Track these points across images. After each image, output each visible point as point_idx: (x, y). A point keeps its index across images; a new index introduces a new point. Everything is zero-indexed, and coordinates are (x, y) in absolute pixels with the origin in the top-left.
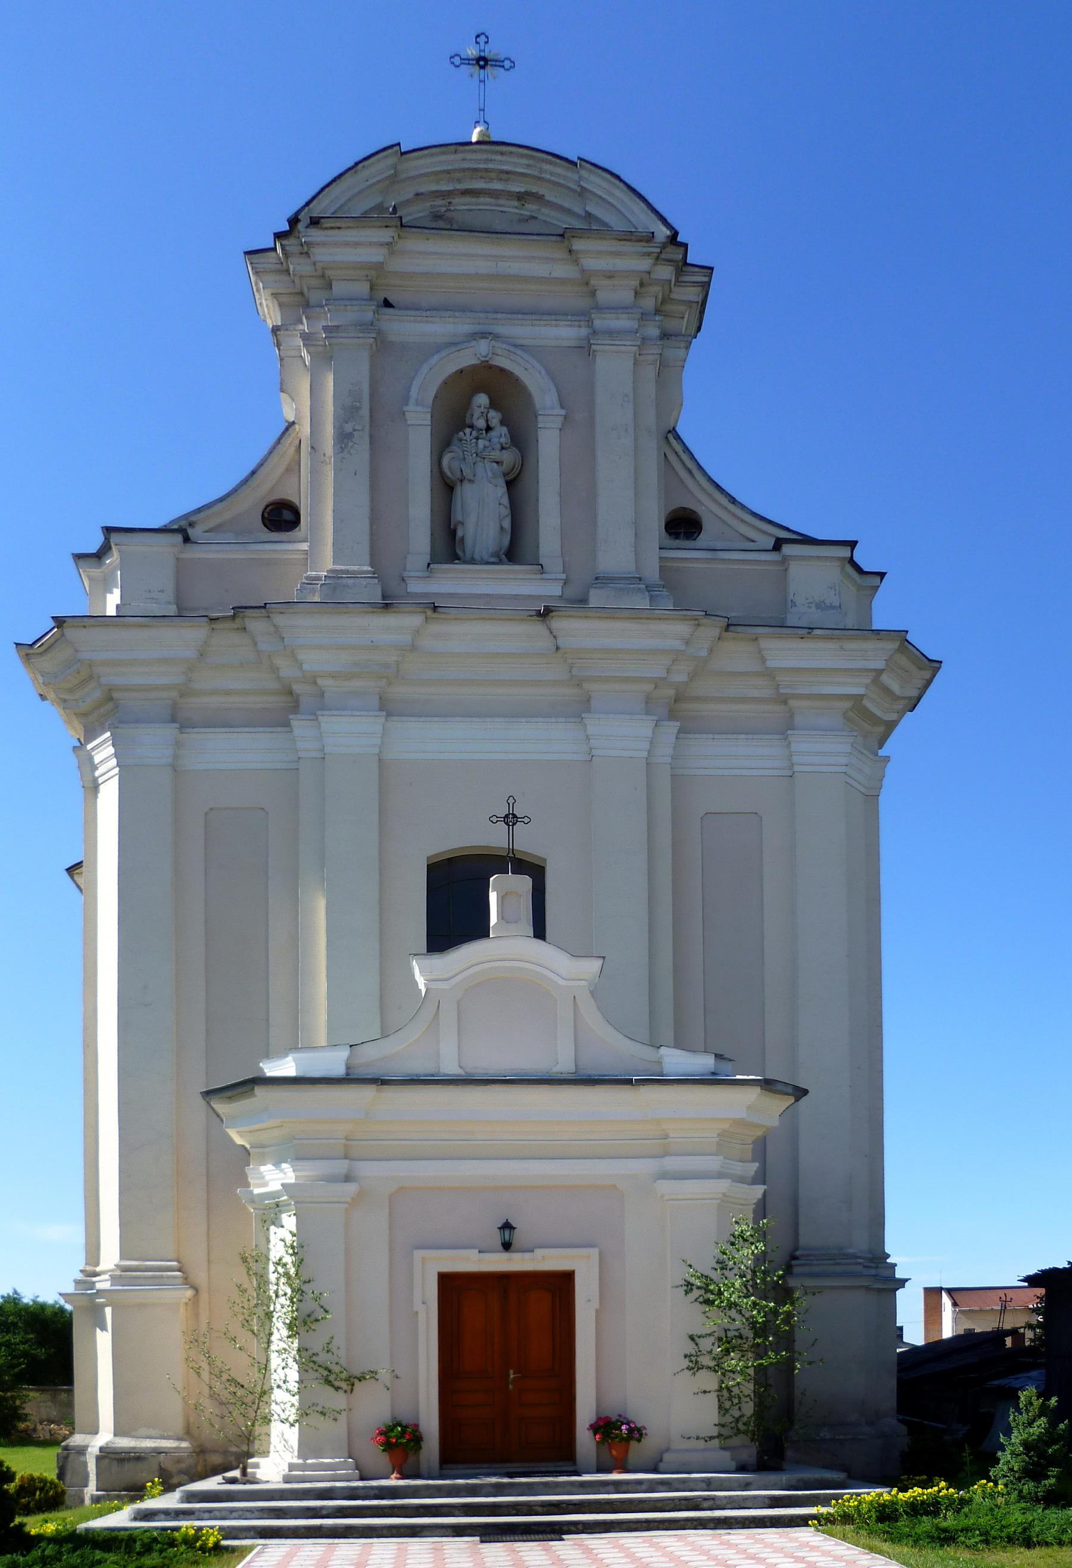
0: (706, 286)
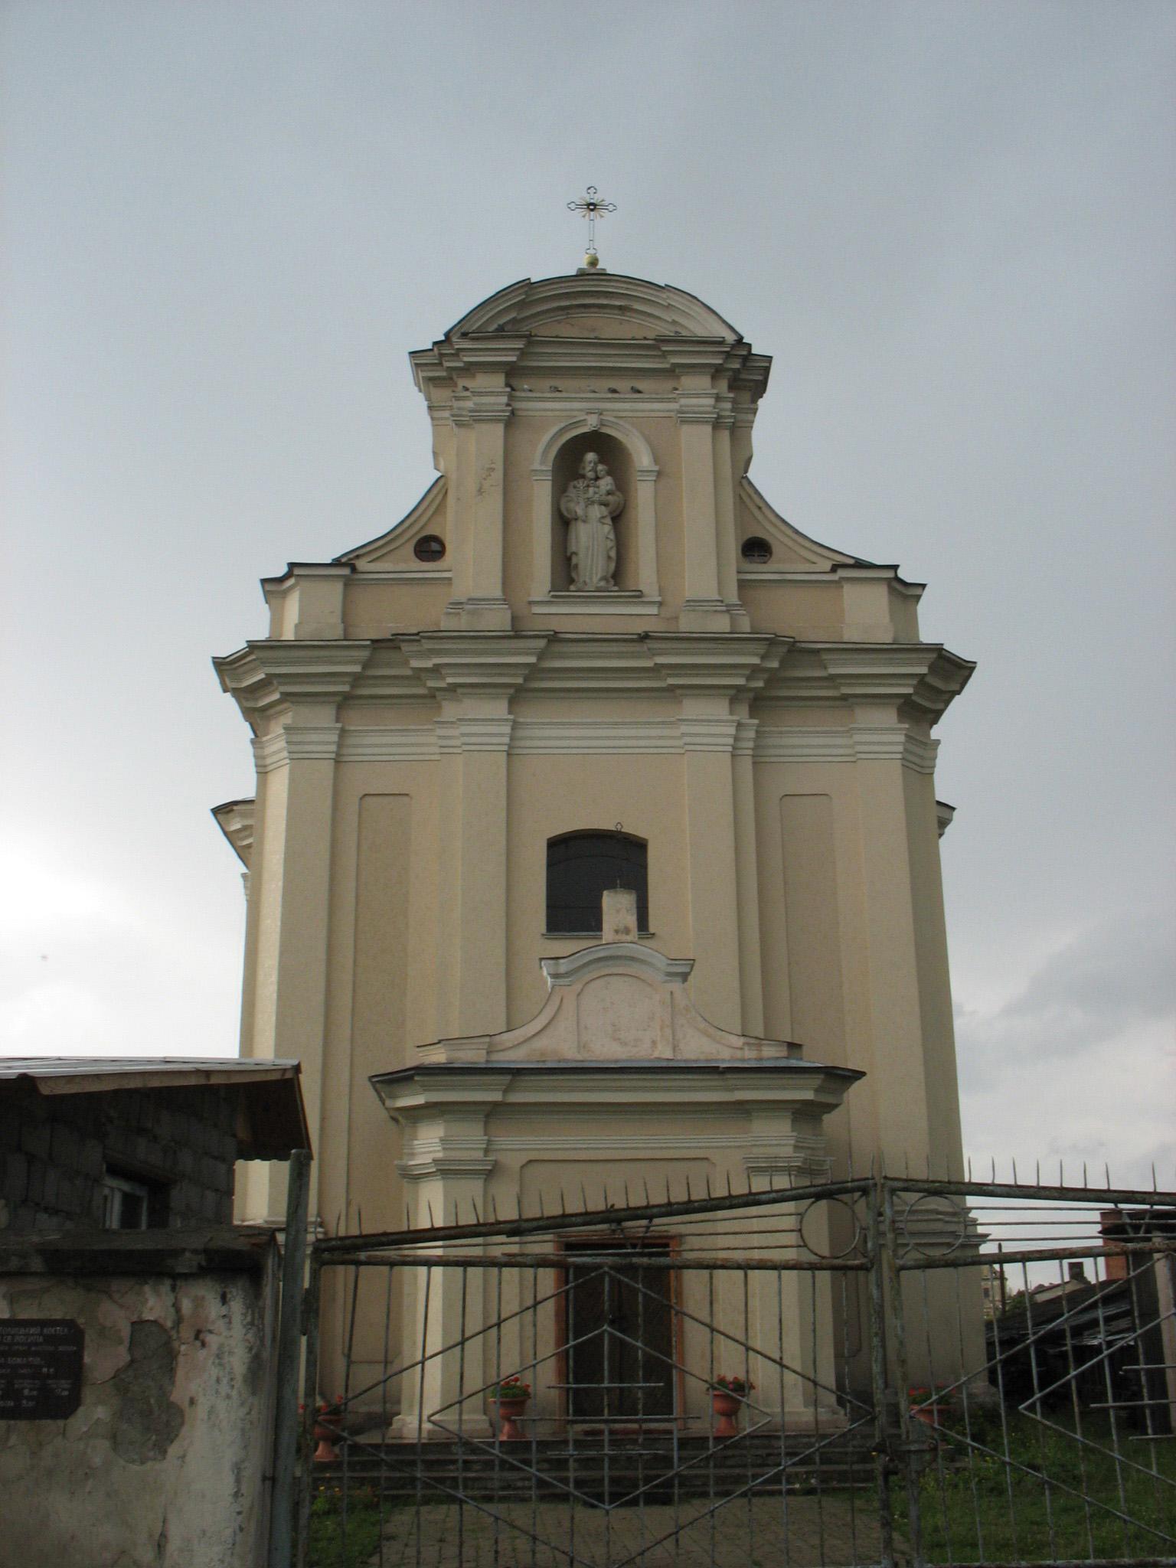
0: (767, 370)
